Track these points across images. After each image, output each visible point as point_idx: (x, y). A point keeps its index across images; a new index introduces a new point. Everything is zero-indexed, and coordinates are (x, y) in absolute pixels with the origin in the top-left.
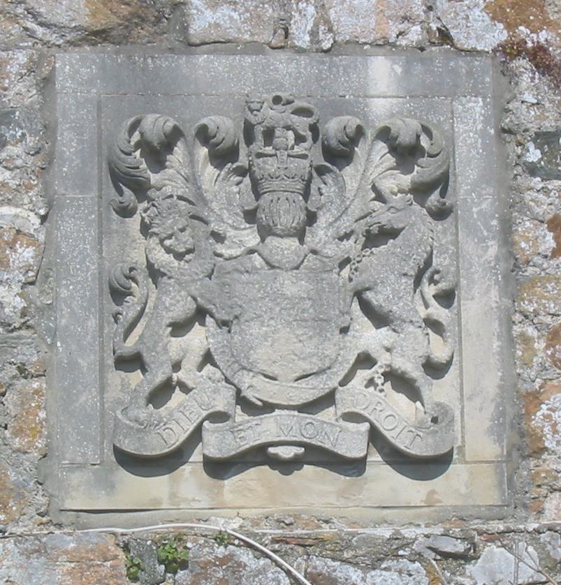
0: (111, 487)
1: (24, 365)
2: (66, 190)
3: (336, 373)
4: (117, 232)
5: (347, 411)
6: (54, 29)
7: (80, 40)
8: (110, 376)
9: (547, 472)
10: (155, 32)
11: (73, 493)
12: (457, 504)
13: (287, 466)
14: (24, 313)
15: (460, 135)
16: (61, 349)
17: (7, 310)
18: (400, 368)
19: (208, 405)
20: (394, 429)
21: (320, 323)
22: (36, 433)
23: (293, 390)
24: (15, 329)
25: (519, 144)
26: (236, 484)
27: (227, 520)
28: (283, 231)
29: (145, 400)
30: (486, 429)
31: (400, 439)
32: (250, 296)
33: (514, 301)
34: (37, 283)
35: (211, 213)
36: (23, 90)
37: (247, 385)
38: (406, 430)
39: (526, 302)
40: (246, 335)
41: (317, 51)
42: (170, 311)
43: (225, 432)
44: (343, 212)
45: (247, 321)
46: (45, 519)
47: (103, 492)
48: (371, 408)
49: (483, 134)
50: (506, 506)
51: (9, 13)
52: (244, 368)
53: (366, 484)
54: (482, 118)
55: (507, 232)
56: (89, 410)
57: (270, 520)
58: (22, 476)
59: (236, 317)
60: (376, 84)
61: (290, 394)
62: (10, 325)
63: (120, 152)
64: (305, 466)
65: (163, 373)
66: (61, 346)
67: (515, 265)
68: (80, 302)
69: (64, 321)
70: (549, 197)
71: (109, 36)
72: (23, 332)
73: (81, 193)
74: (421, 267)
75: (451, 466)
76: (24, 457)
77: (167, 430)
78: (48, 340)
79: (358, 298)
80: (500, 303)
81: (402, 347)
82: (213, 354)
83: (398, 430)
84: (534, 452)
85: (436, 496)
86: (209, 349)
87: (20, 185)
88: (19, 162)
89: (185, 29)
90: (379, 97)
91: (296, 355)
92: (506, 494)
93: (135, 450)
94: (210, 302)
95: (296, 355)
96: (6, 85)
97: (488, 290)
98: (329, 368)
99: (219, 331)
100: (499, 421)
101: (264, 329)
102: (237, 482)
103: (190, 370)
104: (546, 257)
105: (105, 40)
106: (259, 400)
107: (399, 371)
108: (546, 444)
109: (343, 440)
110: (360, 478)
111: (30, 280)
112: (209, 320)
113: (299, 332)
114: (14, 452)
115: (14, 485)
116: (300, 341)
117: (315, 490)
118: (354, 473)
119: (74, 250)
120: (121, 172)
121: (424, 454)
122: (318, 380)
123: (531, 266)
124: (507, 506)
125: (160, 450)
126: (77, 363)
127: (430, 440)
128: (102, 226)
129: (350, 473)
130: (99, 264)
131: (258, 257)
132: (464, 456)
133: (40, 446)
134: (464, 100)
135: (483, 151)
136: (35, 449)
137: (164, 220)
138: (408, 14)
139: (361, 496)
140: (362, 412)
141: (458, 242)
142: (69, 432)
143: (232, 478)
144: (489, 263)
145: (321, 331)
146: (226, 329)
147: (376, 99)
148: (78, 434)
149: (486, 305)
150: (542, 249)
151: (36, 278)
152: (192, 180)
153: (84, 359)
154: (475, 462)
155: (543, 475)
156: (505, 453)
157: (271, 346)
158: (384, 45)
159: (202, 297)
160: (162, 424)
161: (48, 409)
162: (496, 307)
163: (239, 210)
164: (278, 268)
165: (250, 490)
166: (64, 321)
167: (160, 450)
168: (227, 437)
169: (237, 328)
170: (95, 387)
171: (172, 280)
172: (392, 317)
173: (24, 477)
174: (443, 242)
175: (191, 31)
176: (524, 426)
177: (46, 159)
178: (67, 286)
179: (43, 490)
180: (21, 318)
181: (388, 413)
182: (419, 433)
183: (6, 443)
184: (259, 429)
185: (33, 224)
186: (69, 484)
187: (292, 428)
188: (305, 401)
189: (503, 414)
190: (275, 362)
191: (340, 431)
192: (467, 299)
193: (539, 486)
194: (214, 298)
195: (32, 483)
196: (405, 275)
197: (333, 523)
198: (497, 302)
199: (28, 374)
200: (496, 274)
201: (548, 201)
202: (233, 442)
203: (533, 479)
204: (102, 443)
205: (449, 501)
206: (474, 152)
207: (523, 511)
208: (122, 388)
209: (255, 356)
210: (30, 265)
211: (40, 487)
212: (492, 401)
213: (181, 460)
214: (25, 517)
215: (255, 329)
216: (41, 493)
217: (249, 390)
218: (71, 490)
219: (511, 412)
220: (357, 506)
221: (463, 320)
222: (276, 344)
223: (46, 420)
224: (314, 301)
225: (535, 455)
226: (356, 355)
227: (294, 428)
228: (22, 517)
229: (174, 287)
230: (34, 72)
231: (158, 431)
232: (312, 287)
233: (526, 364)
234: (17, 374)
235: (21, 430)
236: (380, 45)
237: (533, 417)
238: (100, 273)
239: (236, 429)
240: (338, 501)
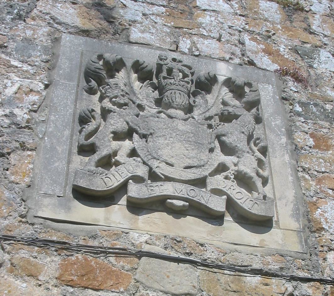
0: (69, 209)
1: (24, 143)
2: (60, 79)
3: (207, 169)
4: (85, 99)
5: (213, 187)
6: (63, 25)
7: (75, 33)
8: (74, 157)
9: (326, 239)
10: (113, 38)
11: (44, 209)
12: (278, 248)
13: (178, 213)
14: (28, 122)
15: (263, 96)
16: (47, 141)
17: (18, 118)
18: (243, 170)
19: (132, 171)
20: (241, 199)
21: (198, 145)
22: (25, 175)
23: (183, 172)
24: (21, 128)
25: (291, 104)
26: (146, 219)
27: (140, 234)
28: (177, 105)
29: (95, 163)
30: (290, 214)
31: (245, 204)
32: (159, 127)
33: (297, 162)
34: (38, 112)
35: (138, 100)
36: (44, 40)
37: (156, 166)
38: (249, 200)
39: (304, 163)
40: (157, 143)
41: (192, 55)
42: (113, 125)
43: (142, 186)
44: (207, 111)
45: (157, 137)
46: (23, 220)
47: (63, 211)
48: (227, 188)
49: (273, 97)
50: (305, 253)
51: (41, 17)
52: (155, 158)
53: (224, 230)
54: (272, 92)
55: (290, 134)
56: (59, 170)
57: (167, 238)
58: (12, 195)
59: (151, 134)
60: (220, 71)
61: (181, 174)
62: (19, 125)
63: (91, 62)
64: (188, 216)
65: (107, 150)
66: (47, 140)
67: (296, 148)
68: (61, 123)
69: (50, 129)
70: (308, 126)
71: (90, 34)
72: (26, 130)
73: (68, 81)
74: (250, 134)
75: (272, 229)
76: (16, 185)
77: (107, 178)
78: (40, 136)
79: (218, 139)
80: (290, 162)
81: (244, 161)
82: (137, 149)
83: (244, 200)
84: (317, 230)
85: (265, 243)
86: (134, 147)
87: (35, 73)
88: (37, 63)
89: (128, 36)
90: (222, 76)
91: (185, 156)
92: (305, 247)
93: (86, 186)
94: (136, 125)
95: (185, 156)
96: (35, 37)
97: (283, 155)
98: (203, 166)
99: (141, 140)
100: (296, 212)
101: (167, 141)
102: (146, 218)
103: (123, 156)
104: (310, 147)
105: (88, 36)
106: (162, 174)
107: (243, 173)
108: (324, 226)
109: (212, 201)
110: (220, 227)
111: (34, 109)
112: (135, 135)
113: (187, 146)
114: (10, 182)
115: (7, 198)
116: (187, 150)
117: (193, 229)
118: (217, 224)
119: (61, 102)
120: (91, 71)
121: (260, 214)
122: (197, 170)
123: (303, 150)
124: (306, 253)
125: (102, 189)
126: (55, 148)
127: (263, 207)
128: (77, 96)
129: (215, 223)
130: (74, 110)
131: (163, 114)
132: (279, 226)
133: (27, 181)
134: (263, 84)
135: (274, 103)
136: (23, 182)
137: (113, 90)
138: (234, 52)
139: (221, 236)
140: (223, 189)
141: (266, 134)
142: (45, 178)
143: (144, 215)
144: (283, 144)
145: (198, 147)
146: (144, 140)
147: (221, 76)
148: (51, 180)
149: (283, 161)
150: (308, 144)
151: (38, 109)
152: (129, 84)
153: (60, 147)
154: (286, 229)
155: (324, 241)
156: (302, 228)
157: (171, 149)
158: (223, 60)
159: (132, 122)
160: (104, 174)
161: (35, 165)
162: (289, 163)
163: (152, 100)
164: (175, 118)
165: (155, 223)
166: (50, 129)
167: (102, 189)
168: (143, 188)
169: (151, 140)
170: (65, 160)
171: (116, 113)
172: (237, 149)
173: (14, 196)
174: (259, 132)
175: (131, 37)
176: (310, 217)
177: (51, 65)
178: (55, 116)
179: (25, 205)
180: (26, 123)
181: (238, 191)
182: (256, 202)
183: (6, 177)
184: (162, 188)
185: (40, 87)
186: (42, 204)
187: (182, 190)
188: (190, 179)
189: (298, 209)
190: (173, 157)
191: (210, 196)
192: (273, 157)
193: (322, 246)
194: (139, 124)
195: (18, 200)
196: (243, 133)
197: (206, 247)
198: (288, 161)
199: (26, 148)
200: (287, 149)
201: (308, 127)
202: (147, 191)
203: (318, 242)
204: (65, 187)
205: (273, 246)
206: (269, 103)
207: (315, 257)
208: (81, 164)
209: (161, 153)
210: (35, 102)
211: (23, 203)
212: (292, 202)
213: (113, 203)
214: (11, 217)
215: (161, 141)
216: (23, 206)
217: (156, 169)
218: (42, 206)
219: (302, 210)
220: (219, 241)
221: (272, 165)
222: (173, 149)
223: (32, 169)
224: (194, 134)
225: (318, 232)
226: (218, 163)
227: (183, 190)
228: (9, 217)
229: (116, 116)
230: (51, 36)
231: (102, 177)
232: (193, 129)
233: (307, 189)
234: (18, 147)
235: (17, 172)
236: (221, 60)
237: (314, 213)
238: (74, 113)
239: (148, 185)
240: (208, 237)
